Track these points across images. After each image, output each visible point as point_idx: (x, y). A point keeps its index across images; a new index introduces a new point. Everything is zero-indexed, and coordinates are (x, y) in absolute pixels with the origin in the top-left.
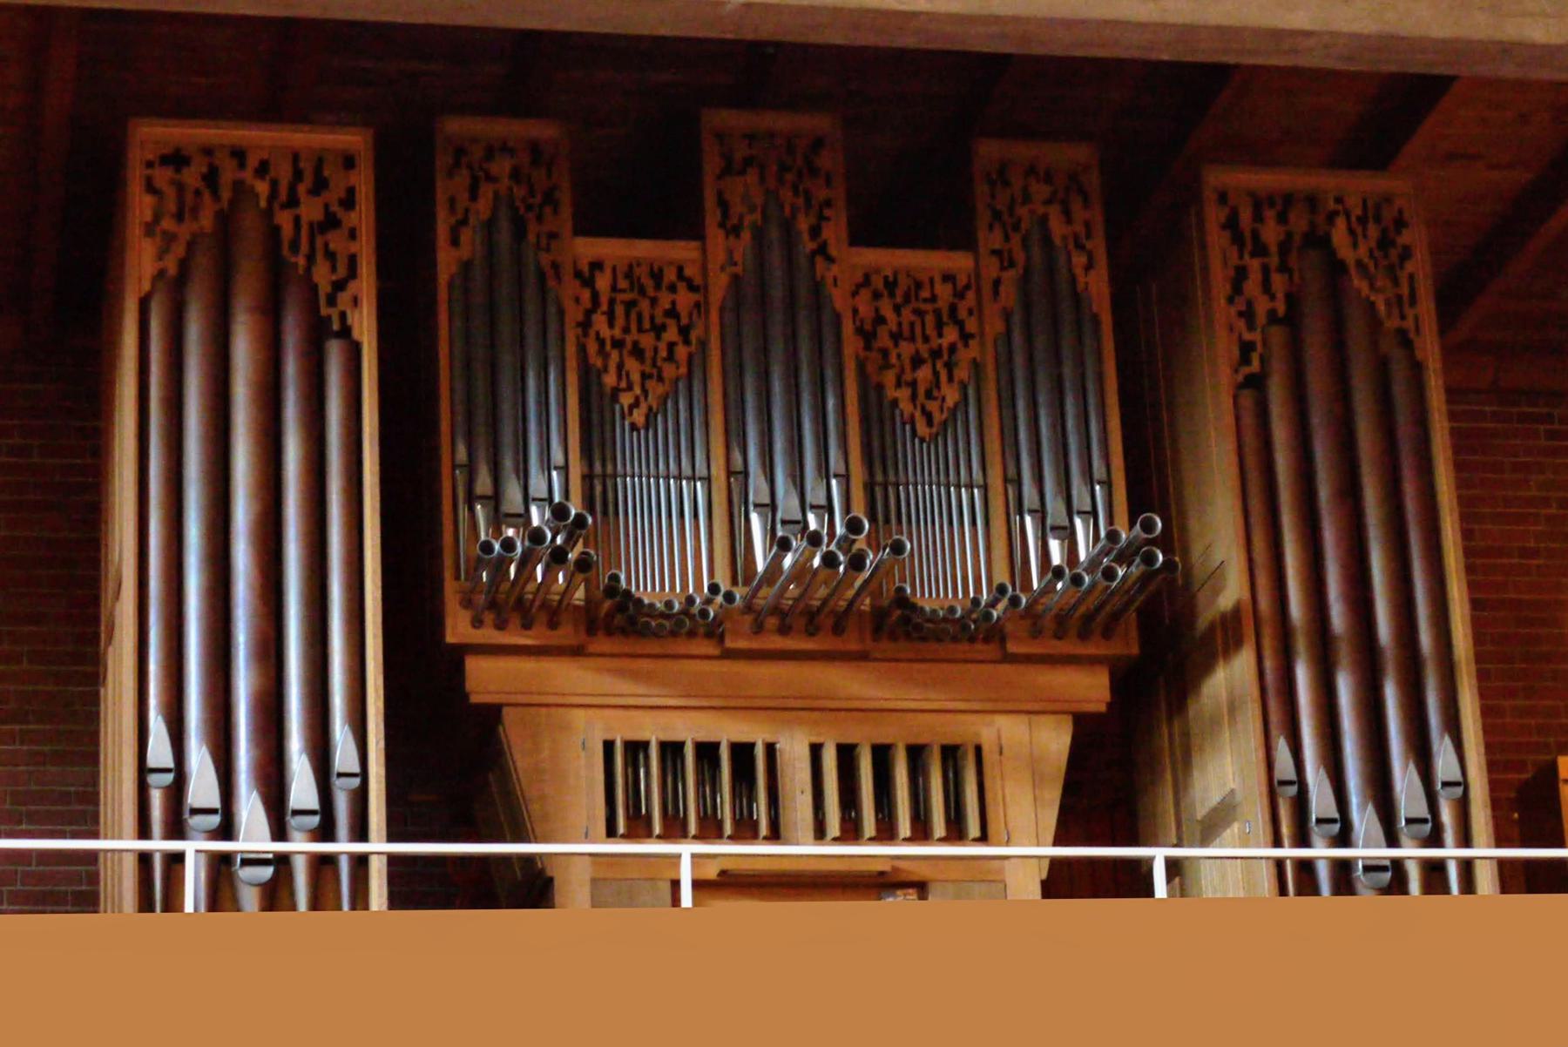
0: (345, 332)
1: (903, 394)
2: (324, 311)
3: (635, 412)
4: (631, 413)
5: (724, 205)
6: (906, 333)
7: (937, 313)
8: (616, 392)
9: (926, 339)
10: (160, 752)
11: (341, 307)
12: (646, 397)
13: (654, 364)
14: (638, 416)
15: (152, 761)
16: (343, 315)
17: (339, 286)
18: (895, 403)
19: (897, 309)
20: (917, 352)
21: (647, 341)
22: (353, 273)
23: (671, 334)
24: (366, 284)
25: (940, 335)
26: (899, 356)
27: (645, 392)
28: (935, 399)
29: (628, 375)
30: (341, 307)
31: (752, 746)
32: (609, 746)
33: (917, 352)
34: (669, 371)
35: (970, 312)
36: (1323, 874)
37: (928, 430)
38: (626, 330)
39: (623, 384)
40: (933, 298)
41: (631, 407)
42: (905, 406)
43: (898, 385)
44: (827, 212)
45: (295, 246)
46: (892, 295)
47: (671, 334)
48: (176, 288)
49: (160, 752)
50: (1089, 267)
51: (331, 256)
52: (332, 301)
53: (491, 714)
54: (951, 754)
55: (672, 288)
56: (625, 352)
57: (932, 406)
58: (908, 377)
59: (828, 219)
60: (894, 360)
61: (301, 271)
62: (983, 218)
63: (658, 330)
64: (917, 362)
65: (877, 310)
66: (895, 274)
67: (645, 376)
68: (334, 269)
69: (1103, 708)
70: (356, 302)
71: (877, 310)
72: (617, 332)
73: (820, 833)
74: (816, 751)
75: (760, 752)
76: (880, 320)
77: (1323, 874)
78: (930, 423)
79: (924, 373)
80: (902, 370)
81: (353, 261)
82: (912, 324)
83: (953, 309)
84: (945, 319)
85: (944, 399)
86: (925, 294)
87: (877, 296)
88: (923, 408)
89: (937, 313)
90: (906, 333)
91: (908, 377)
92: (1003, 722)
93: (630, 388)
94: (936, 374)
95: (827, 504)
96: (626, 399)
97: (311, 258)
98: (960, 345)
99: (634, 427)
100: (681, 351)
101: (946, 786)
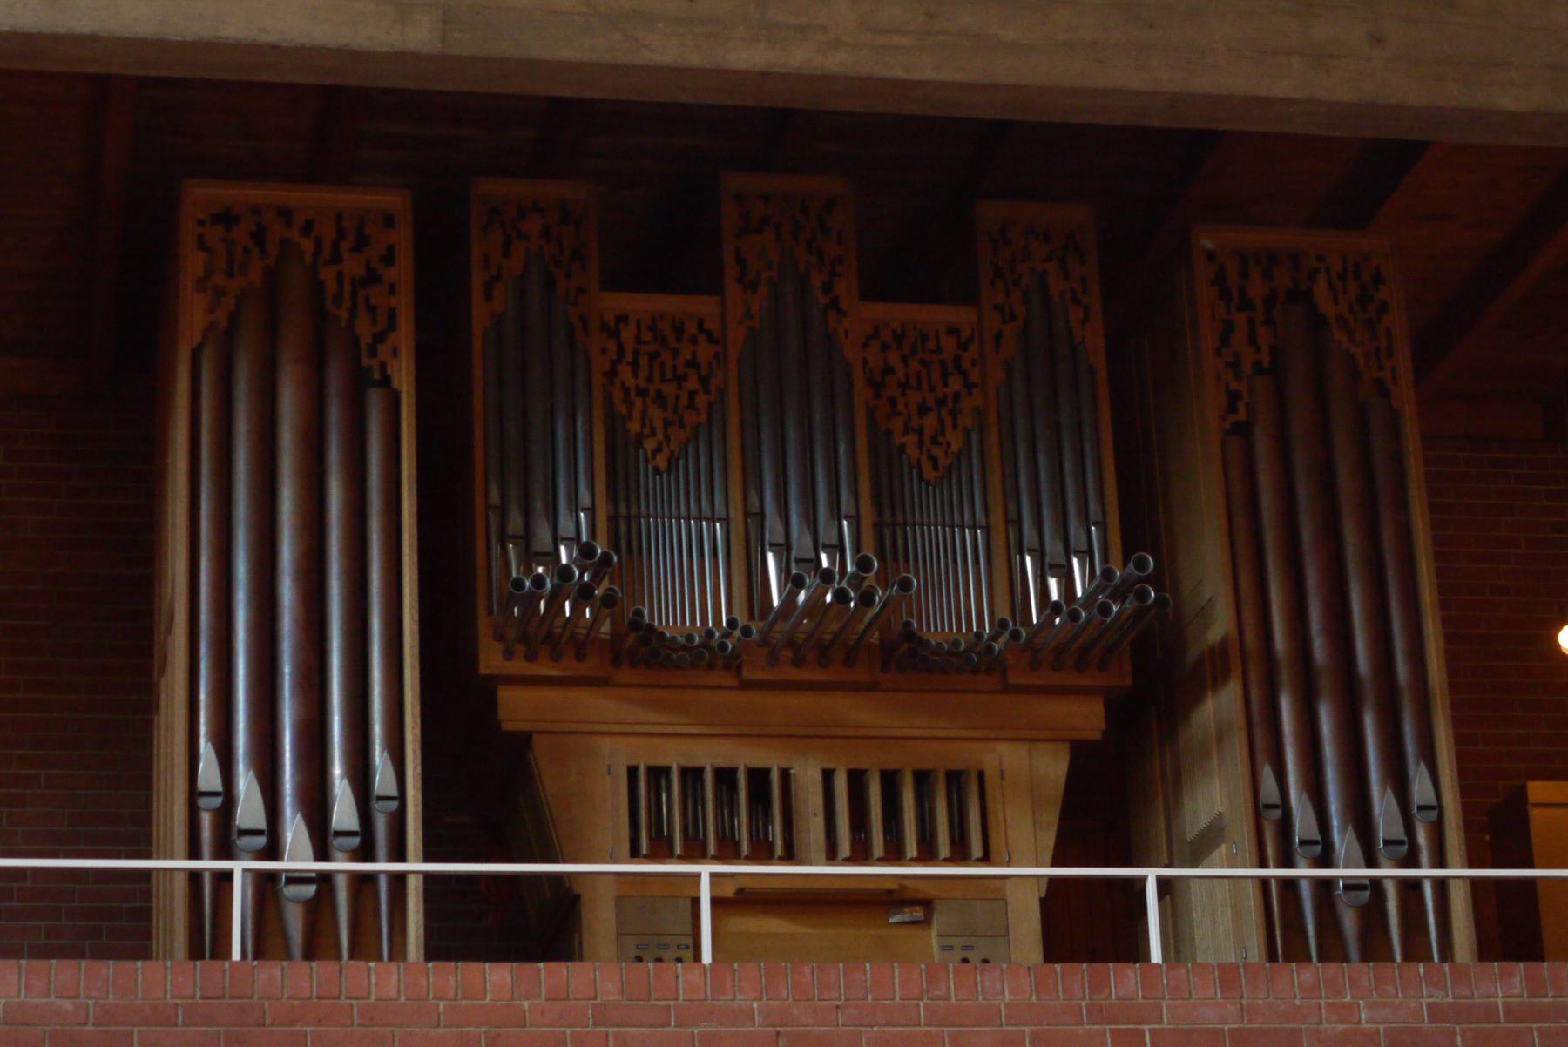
0: (385, 381)
1: (910, 440)
2: (365, 361)
6: (913, 383)
14: (661, 460)
16: (383, 366)
17: (380, 338)
19: (905, 359)
21: (669, 390)
22: (392, 324)
23: (693, 383)
25: (946, 385)
27: (667, 437)
32: (632, 772)
34: (690, 418)
38: (650, 380)
39: (647, 431)
40: (939, 350)
42: (912, 450)
43: (906, 431)
47: (693, 383)
50: (1085, 320)
51: (372, 310)
52: (373, 352)
54: (955, 779)
55: (694, 341)
57: (937, 452)
58: (915, 424)
61: (343, 324)
63: (680, 379)
64: (923, 409)
67: (667, 423)
68: (374, 322)
70: (395, 353)
74: (828, 776)
76: (888, 370)
78: (935, 468)
79: (930, 421)
81: (392, 315)
82: (919, 375)
83: (957, 360)
85: (948, 445)
86: (931, 345)
87: (885, 347)
92: (1003, 748)
93: (653, 433)
94: (941, 422)
97: (353, 311)
99: (657, 471)
100: (702, 400)
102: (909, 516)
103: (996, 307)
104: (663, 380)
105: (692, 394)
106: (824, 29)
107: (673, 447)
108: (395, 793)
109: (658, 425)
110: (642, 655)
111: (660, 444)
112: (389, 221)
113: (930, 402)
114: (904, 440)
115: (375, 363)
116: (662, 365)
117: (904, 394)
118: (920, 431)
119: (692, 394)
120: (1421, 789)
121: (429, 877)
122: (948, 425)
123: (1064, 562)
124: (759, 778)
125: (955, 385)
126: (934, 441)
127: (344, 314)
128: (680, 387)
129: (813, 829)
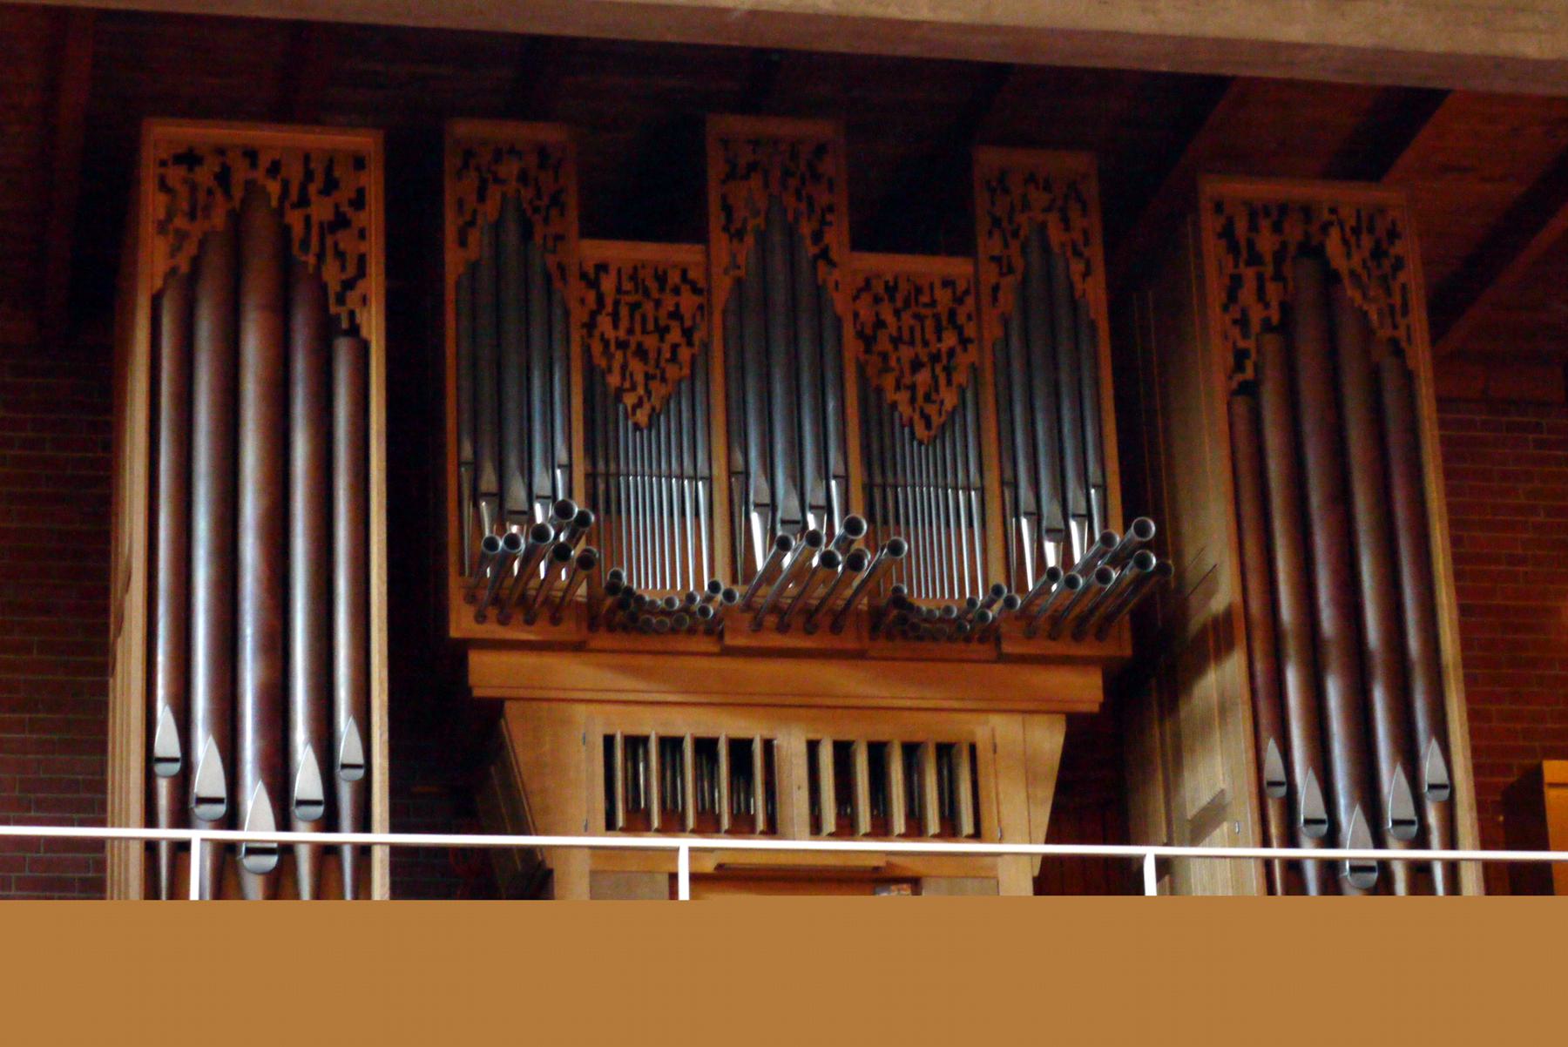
0: (354, 330)
1: (902, 397)
2: (333, 309)
3: (638, 412)
4: (634, 413)
5: (728, 209)
6: (906, 337)
7: (937, 317)
9: (926, 343)
14: (642, 416)
16: (352, 314)
17: (349, 285)
20: (917, 355)
22: (362, 272)
23: (675, 336)
25: (940, 339)
26: (898, 359)
27: (649, 393)
30: (350, 306)
31: (749, 742)
32: (609, 741)
33: (917, 355)
34: (672, 372)
35: (969, 317)
38: (630, 331)
39: (627, 385)
42: (904, 409)
43: (898, 388)
44: (829, 217)
45: (305, 244)
46: (892, 299)
47: (675, 336)
50: (1086, 274)
51: (340, 255)
52: (341, 300)
54: (945, 751)
55: (676, 291)
56: (629, 353)
57: (931, 409)
58: (907, 380)
59: (830, 224)
60: (893, 363)
61: (311, 269)
62: (983, 225)
63: (662, 331)
64: (916, 366)
65: (877, 314)
66: (896, 279)
67: (648, 377)
68: (343, 268)
70: (364, 300)
71: (877, 314)
72: (622, 333)
74: (813, 747)
75: (757, 748)
76: (880, 324)
78: (928, 426)
79: (923, 377)
81: (362, 260)
82: (912, 329)
83: (952, 314)
84: (944, 323)
85: (942, 402)
86: (925, 299)
87: (877, 300)
89: (937, 317)
90: (906, 337)
92: (997, 721)
93: (633, 388)
94: (935, 378)
97: (321, 257)
98: (959, 350)
99: (637, 427)
100: (685, 354)
103: (994, 259)
104: (644, 331)
105: (674, 348)
109: (639, 378)
110: (621, 621)
111: (640, 399)
117: (896, 349)
119: (674, 348)
121: (395, 850)
125: (950, 340)
127: (312, 260)
128: (662, 339)
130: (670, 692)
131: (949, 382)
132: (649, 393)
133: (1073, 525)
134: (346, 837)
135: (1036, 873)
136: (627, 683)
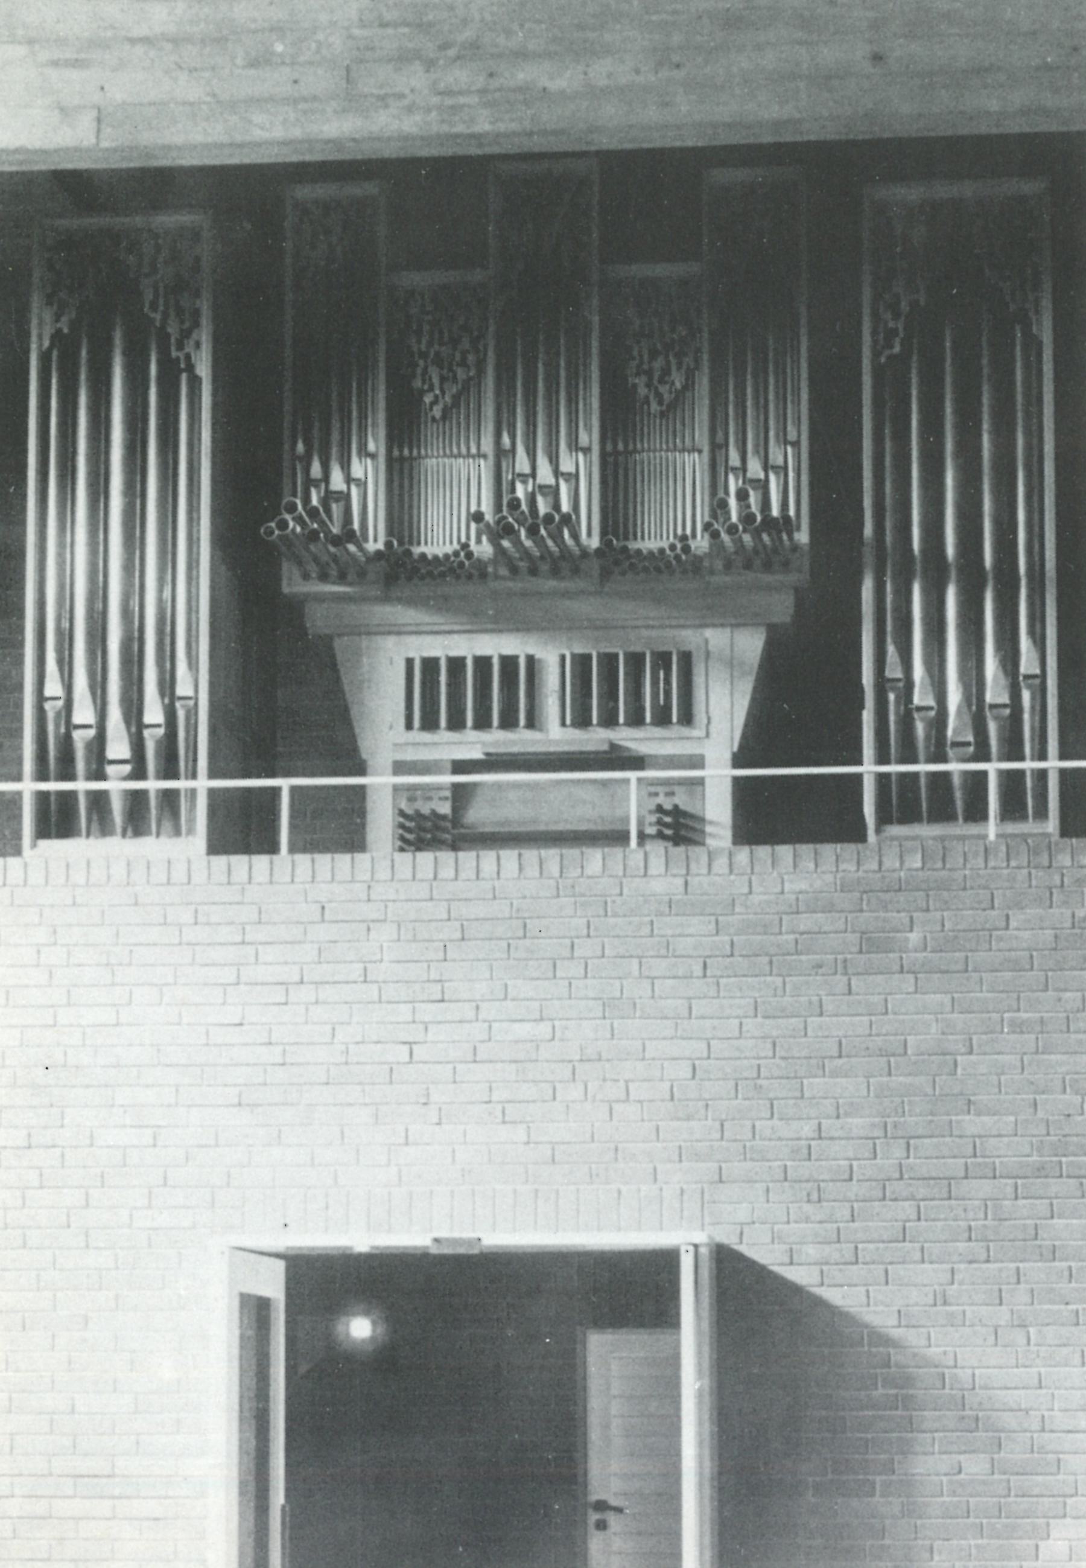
0: (190, 368)
1: (641, 381)
2: (174, 354)
3: (435, 408)
4: (431, 409)
8: (422, 393)
10: (53, 687)
11: (187, 350)
12: (443, 398)
13: (451, 370)
14: (437, 411)
15: (48, 693)
16: (188, 357)
17: (186, 334)
18: (635, 386)
21: (445, 350)
22: (197, 324)
23: (466, 344)
24: (205, 336)
27: (443, 392)
28: (666, 383)
29: (430, 379)
30: (187, 350)
31: (517, 657)
32: (410, 662)
34: (461, 374)
36: (117, 806)
37: (659, 408)
38: (430, 344)
39: (426, 387)
41: (432, 404)
42: (642, 391)
43: (638, 374)
45: (154, 306)
47: (466, 344)
48: (64, 350)
49: (53, 687)
51: (180, 311)
52: (180, 347)
53: (327, 642)
54: (663, 660)
56: (429, 361)
57: (664, 389)
58: (645, 367)
60: (635, 353)
61: (158, 324)
63: (455, 342)
64: (654, 354)
67: (443, 379)
68: (182, 322)
69: (788, 619)
70: (198, 345)
72: (423, 347)
73: (582, 721)
74: (563, 658)
75: (522, 662)
77: (117, 806)
78: (660, 403)
79: (659, 363)
80: (641, 363)
81: (196, 314)
85: (673, 383)
88: (656, 388)
91: (645, 367)
92: (708, 633)
93: (431, 389)
94: (668, 363)
95: (567, 476)
96: (428, 399)
97: (165, 316)
99: (434, 419)
100: (471, 358)
101: (628, 688)
102: (646, 445)
104: (441, 344)
105: (464, 354)
106: (401, 96)
107: (448, 398)
108: (1038, 671)
109: (436, 381)
110: (404, 572)
111: (436, 397)
112: (196, 235)
113: (659, 346)
114: (637, 381)
115: (181, 355)
116: (441, 332)
117: (638, 342)
118: (649, 373)
119: (464, 354)
120: (1028, 663)
121: (1063, 772)
122: (674, 368)
123: (762, 476)
124: (509, 663)
126: (661, 381)
127: (158, 317)
128: (455, 349)
129: (551, 707)
130: (456, 623)
131: (679, 365)
132: (443, 392)
133: (772, 478)
134: (1028, 765)
135: (735, 749)
136: (437, 619)
